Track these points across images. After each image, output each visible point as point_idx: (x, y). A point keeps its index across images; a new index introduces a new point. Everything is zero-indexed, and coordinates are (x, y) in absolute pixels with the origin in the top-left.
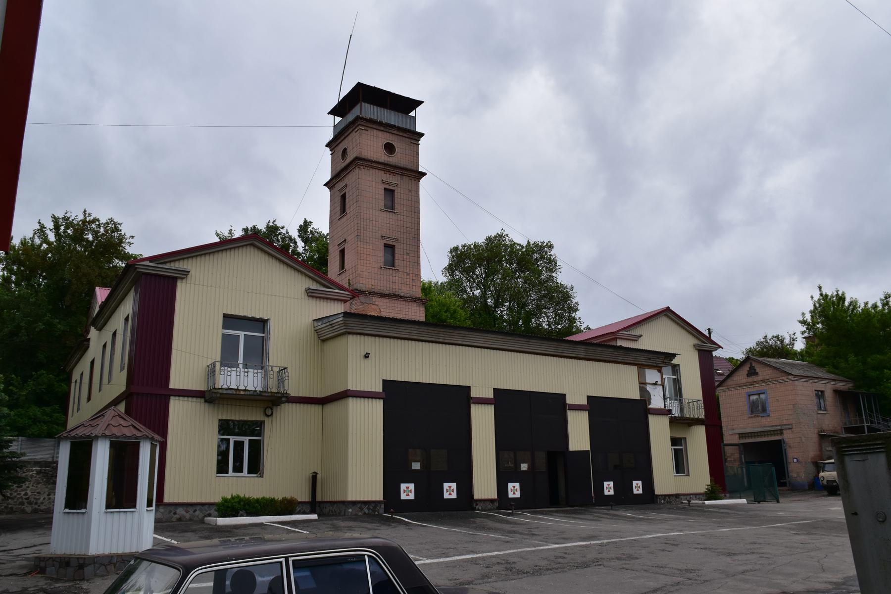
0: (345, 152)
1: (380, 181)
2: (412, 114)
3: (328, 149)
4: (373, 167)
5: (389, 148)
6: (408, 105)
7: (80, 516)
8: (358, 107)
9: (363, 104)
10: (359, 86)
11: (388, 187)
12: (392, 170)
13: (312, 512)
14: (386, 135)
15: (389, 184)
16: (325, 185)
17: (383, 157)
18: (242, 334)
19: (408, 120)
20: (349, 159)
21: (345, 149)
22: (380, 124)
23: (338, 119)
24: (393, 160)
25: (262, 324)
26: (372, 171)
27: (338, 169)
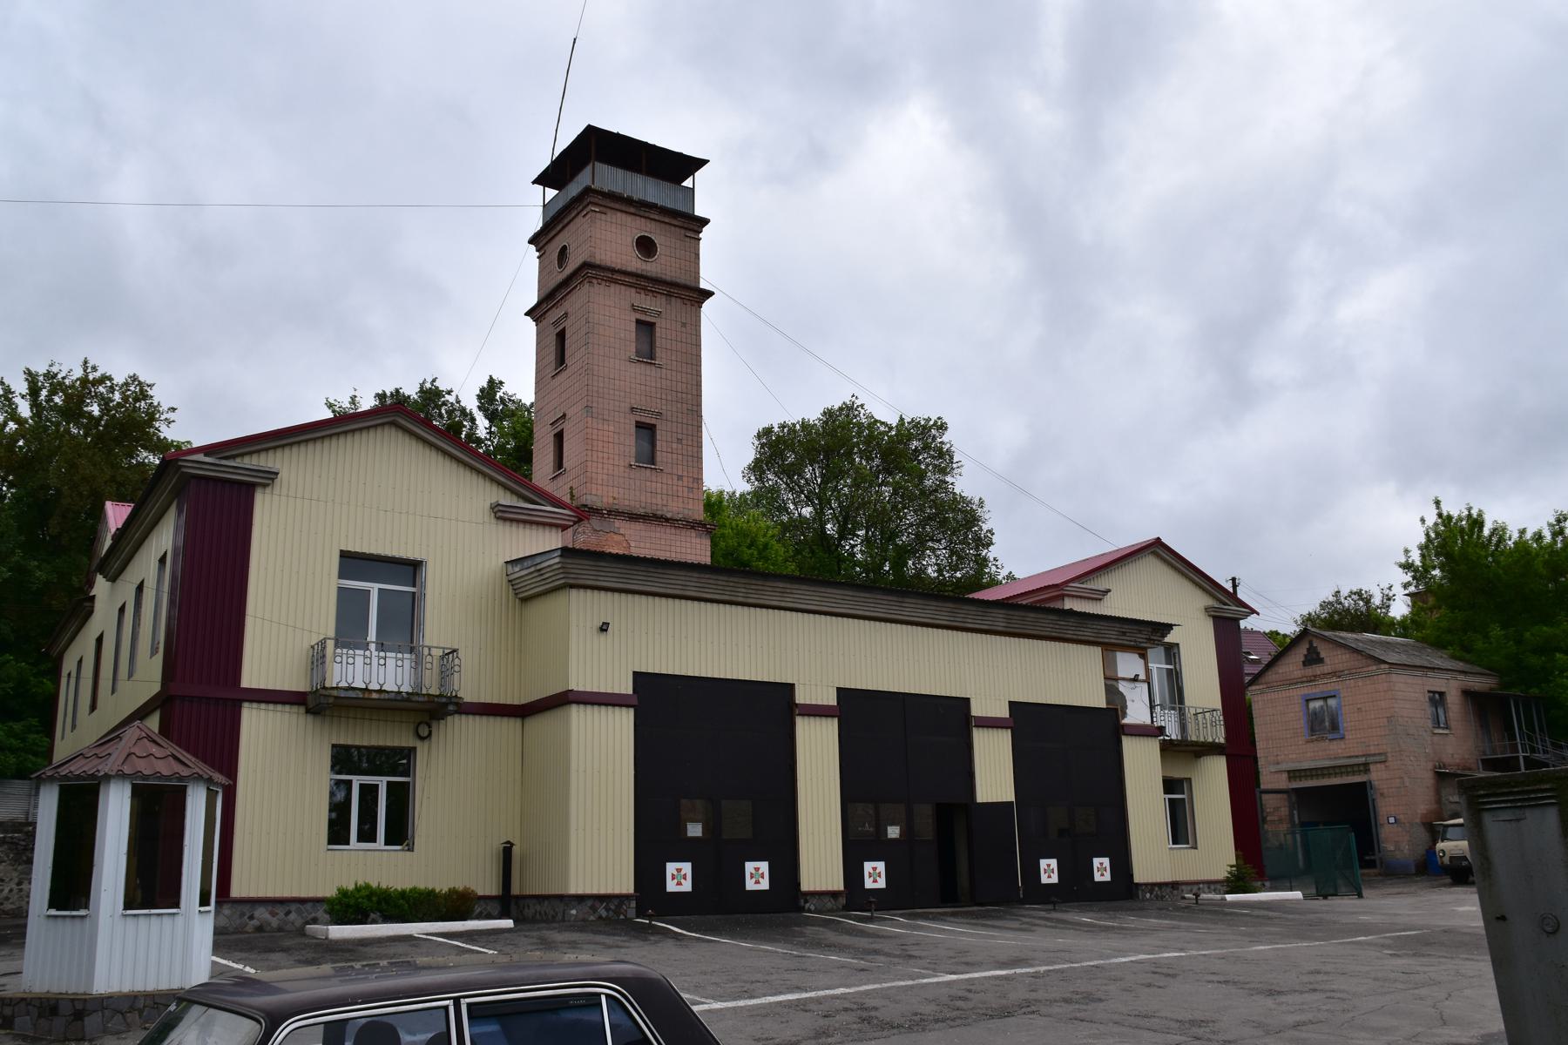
0: (563, 252)
2: (688, 183)
3: (533, 247)
4: (616, 282)
5: (646, 246)
6: (680, 167)
9: (597, 164)
10: (590, 130)
11: (643, 318)
14: (640, 222)
15: (644, 311)
17: (632, 261)
18: (374, 588)
20: (571, 267)
22: (629, 201)
23: (551, 193)
25: (411, 569)
26: (614, 288)
27: (552, 284)
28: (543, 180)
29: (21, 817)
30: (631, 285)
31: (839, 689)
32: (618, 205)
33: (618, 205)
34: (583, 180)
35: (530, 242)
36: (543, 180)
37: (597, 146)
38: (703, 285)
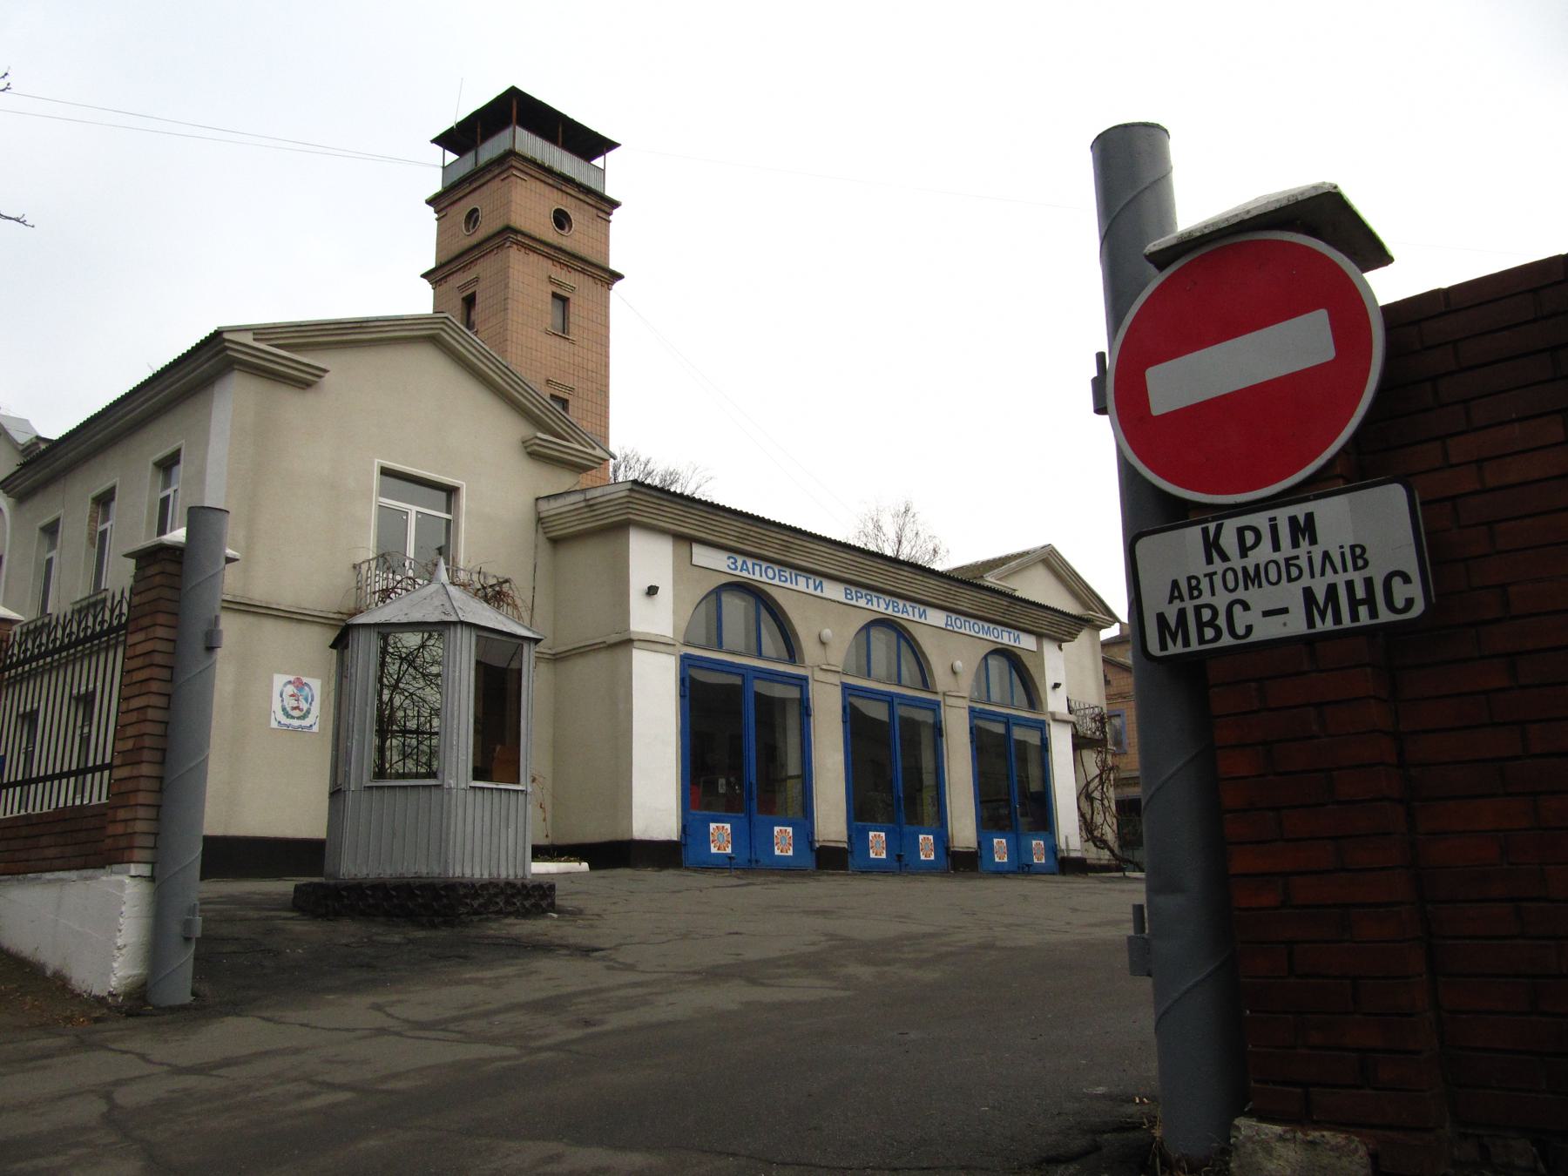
0: (472, 217)
1: (545, 278)
2: (598, 162)
3: (432, 209)
4: (534, 250)
5: (561, 219)
6: (592, 145)
7: (423, 794)
8: (507, 133)
9: (518, 129)
10: (513, 93)
11: (559, 291)
12: (563, 258)
13: (581, 860)
14: (556, 195)
15: (559, 284)
16: (424, 276)
17: (549, 233)
18: (413, 510)
19: (593, 174)
20: (484, 231)
21: (475, 210)
22: (549, 171)
23: (451, 157)
24: (567, 240)
25: (451, 492)
26: (533, 257)
27: (456, 248)
28: (446, 140)
29: (318, 639)
30: (548, 257)
31: (202, 879)
32: (520, 175)
33: (520, 175)
34: (490, 150)
35: (429, 202)
36: (446, 140)
37: (515, 108)
38: (613, 266)
